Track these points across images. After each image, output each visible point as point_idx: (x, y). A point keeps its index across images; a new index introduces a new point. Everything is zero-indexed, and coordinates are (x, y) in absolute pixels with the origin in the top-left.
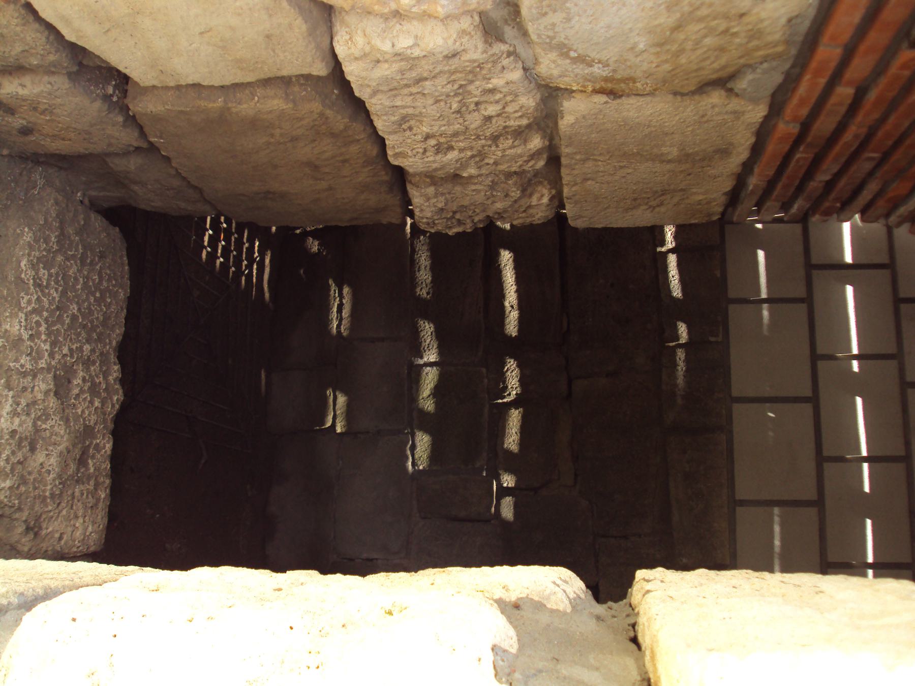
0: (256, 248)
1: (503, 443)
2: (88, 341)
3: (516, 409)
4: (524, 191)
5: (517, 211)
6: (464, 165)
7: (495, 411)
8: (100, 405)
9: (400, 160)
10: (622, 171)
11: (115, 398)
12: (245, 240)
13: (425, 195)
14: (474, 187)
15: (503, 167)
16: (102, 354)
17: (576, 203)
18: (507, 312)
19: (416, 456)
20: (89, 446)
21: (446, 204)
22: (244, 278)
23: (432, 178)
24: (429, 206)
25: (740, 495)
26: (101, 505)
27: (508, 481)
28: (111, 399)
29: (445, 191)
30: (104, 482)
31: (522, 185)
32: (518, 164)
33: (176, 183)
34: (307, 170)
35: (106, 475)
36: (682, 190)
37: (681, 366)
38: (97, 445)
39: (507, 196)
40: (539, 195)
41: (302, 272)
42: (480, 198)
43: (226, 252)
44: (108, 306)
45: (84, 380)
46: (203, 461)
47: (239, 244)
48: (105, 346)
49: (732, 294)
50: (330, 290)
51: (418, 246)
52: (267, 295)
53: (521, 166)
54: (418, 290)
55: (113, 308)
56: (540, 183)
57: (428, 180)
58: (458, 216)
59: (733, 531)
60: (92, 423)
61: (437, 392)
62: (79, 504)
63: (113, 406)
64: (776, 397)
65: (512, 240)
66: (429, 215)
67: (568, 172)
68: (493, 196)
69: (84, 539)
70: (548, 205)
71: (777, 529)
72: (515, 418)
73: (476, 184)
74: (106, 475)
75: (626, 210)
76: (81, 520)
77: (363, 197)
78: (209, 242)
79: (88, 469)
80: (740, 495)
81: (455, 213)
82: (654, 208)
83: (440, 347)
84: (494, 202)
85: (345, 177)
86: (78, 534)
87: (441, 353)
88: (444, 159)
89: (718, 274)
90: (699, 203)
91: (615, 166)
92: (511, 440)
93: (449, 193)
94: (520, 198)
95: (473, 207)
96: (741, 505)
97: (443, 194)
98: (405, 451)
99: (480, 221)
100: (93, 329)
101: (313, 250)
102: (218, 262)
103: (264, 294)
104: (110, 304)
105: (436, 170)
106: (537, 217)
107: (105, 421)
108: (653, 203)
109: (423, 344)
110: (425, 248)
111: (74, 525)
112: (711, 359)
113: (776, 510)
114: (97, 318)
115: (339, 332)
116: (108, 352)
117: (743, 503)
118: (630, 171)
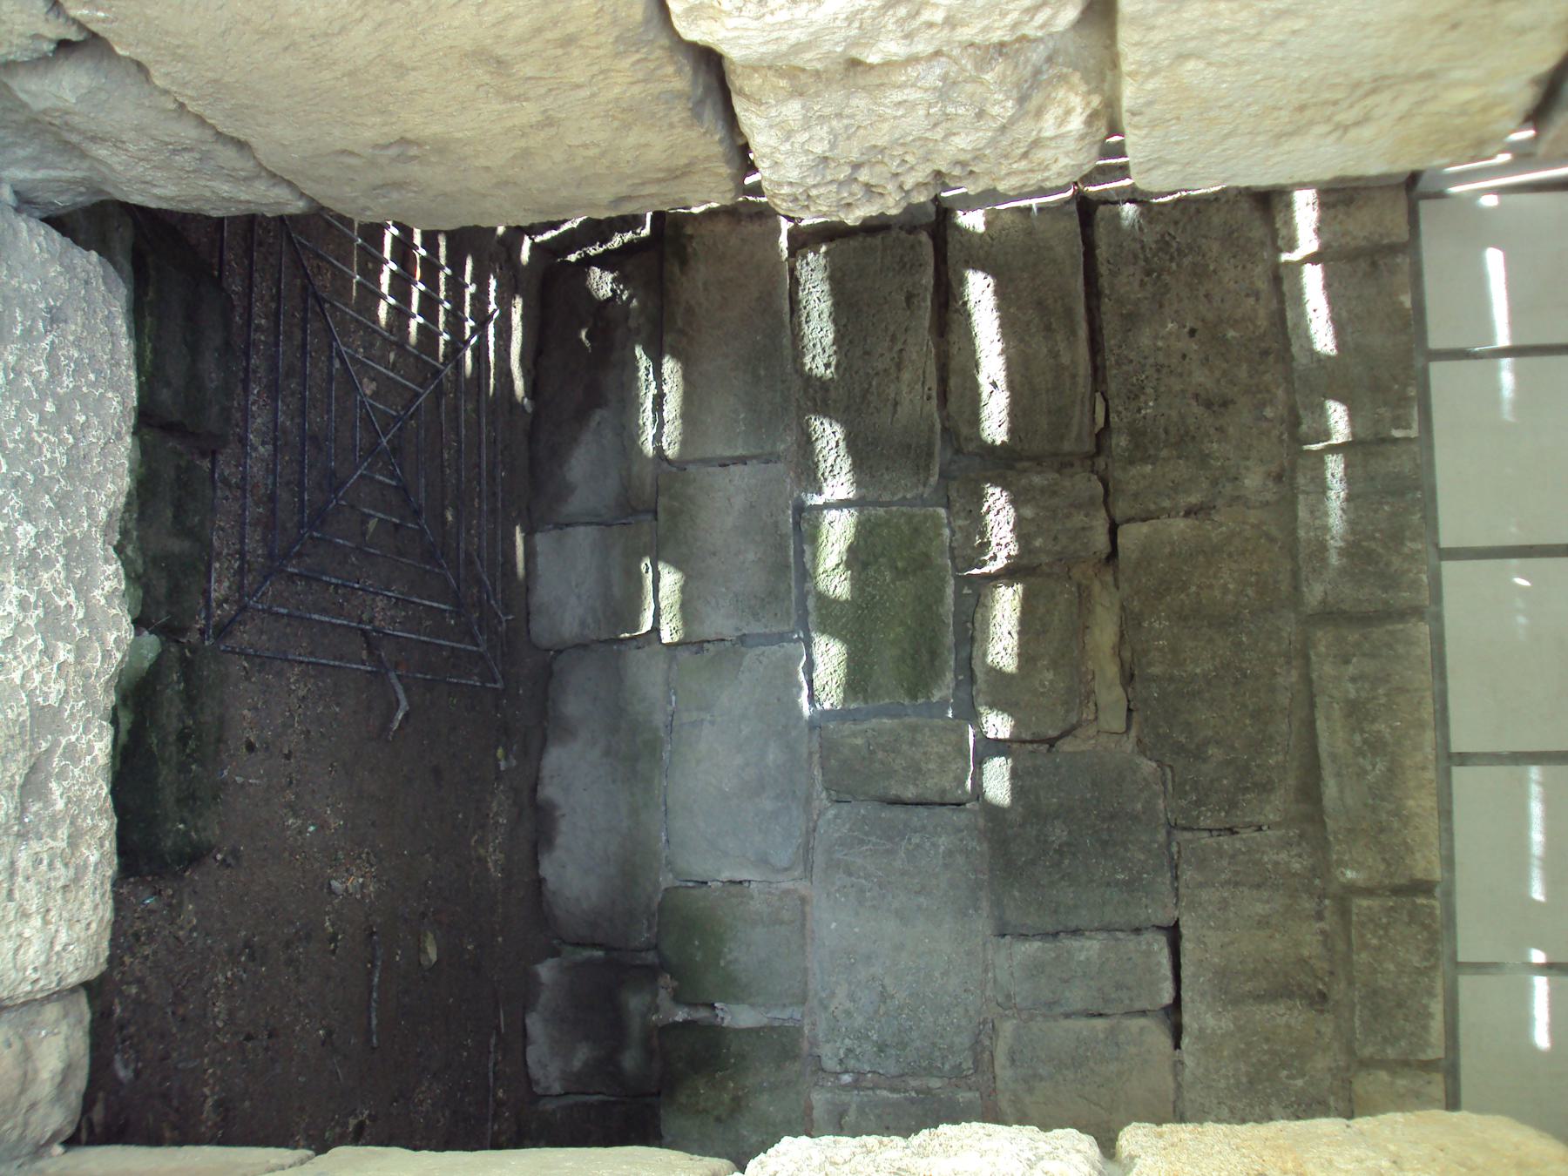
0: (492, 295)
1: (985, 655)
2: (27, 515)
3: (1007, 586)
4: (1022, 100)
5: (1006, 156)
6: (868, 35)
7: (966, 591)
8: (71, 658)
9: (705, 25)
10: (1279, 25)
11: (111, 638)
12: (468, 279)
13: (779, 125)
14: (897, 96)
15: (965, 33)
16: (69, 542)
17: (1153, 124)
18: (984, 396)
19: (817, 684)
20: (49, 752)
21: (833, 145)
22: (468, 353)
23: (794, 75)
24: (791, 153)
25: (1460, 742)
26: (89, 879)
27: (998, 725)
28: (103, 642)
29: (828, 111)
30: (95, 827)
31: (1018, 85)
32: (1009, 19)
33: (188, 132)
34: (481, 74)
35: (100, 811)
36: (1428, 75)
37: (1337, 491)
38: (71, 747)
39: (981, 114)
40: (1060, 111)
41: (583, 334)
42: (915, 123)
43: (429, 305)
44: (80, 432)
45: (23, 604)
46: (400, 715)
47: (456, 286)
48: (78, 524)
49: (1435, 341)
50: (637, 369)
51: (804, 273)
52: (519, 385)
53: (1016, 25)
54: (807, 359)
55: (94, 435)
56: (1062, 78)
57: (783, 83)
58: (864, 176)
59: (1446, 813)
60: (53, 700)
61: (856, 558)
62: (28, 886)
63: (107, 655)
64: (1531, 547)
65: (984, 255)
66: (794, 175)
67: (1136, 38)
68: (948, 117)
69: (48, 962)
70: (1082, 137)
71: (1536, 809)
72: (1006, 604)
73: (901, 86)
74: (100, 811)
75: (1279, 137)
76: (37, 921)
77: (632, 139)
78: (391, 286)
79: (48, 803)
80: (1459, 744)
81: (857, 166)
82: (1346, 128)
83: (857, 467)
84: (949, 134)
85: (578, 86)
86: (33, 953)
87: (858, 483)
88: (813, 16)
89: (1406, 300)
90: (1463, 109)
91: (1261, 13)
92: (999, 647)
93: (839, 116)
94: (1012, 121)
95: (899, 151)
96: (1461, 764)
97: (822, 119)
98: (797, 673)
99: (918, 185)
100: (42, 485)
101: (601, 293)
102: (413, 325)
103: (512, 382)
104: (86, 426)
105: (798, 48)
106: (1055, 168)
107: (87, 691)
108: (1342, 117)
109: (822, 465)
110: (819, 275)
111: (20, 935)
112: (1396, 479)
113: (1535, 772)
114: (52, 462)
115: (659, 450)
116: (87, 536)
117: (1464, 759)
118: (1299, 24)
